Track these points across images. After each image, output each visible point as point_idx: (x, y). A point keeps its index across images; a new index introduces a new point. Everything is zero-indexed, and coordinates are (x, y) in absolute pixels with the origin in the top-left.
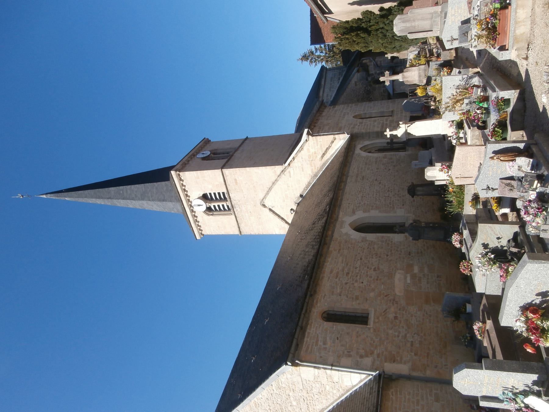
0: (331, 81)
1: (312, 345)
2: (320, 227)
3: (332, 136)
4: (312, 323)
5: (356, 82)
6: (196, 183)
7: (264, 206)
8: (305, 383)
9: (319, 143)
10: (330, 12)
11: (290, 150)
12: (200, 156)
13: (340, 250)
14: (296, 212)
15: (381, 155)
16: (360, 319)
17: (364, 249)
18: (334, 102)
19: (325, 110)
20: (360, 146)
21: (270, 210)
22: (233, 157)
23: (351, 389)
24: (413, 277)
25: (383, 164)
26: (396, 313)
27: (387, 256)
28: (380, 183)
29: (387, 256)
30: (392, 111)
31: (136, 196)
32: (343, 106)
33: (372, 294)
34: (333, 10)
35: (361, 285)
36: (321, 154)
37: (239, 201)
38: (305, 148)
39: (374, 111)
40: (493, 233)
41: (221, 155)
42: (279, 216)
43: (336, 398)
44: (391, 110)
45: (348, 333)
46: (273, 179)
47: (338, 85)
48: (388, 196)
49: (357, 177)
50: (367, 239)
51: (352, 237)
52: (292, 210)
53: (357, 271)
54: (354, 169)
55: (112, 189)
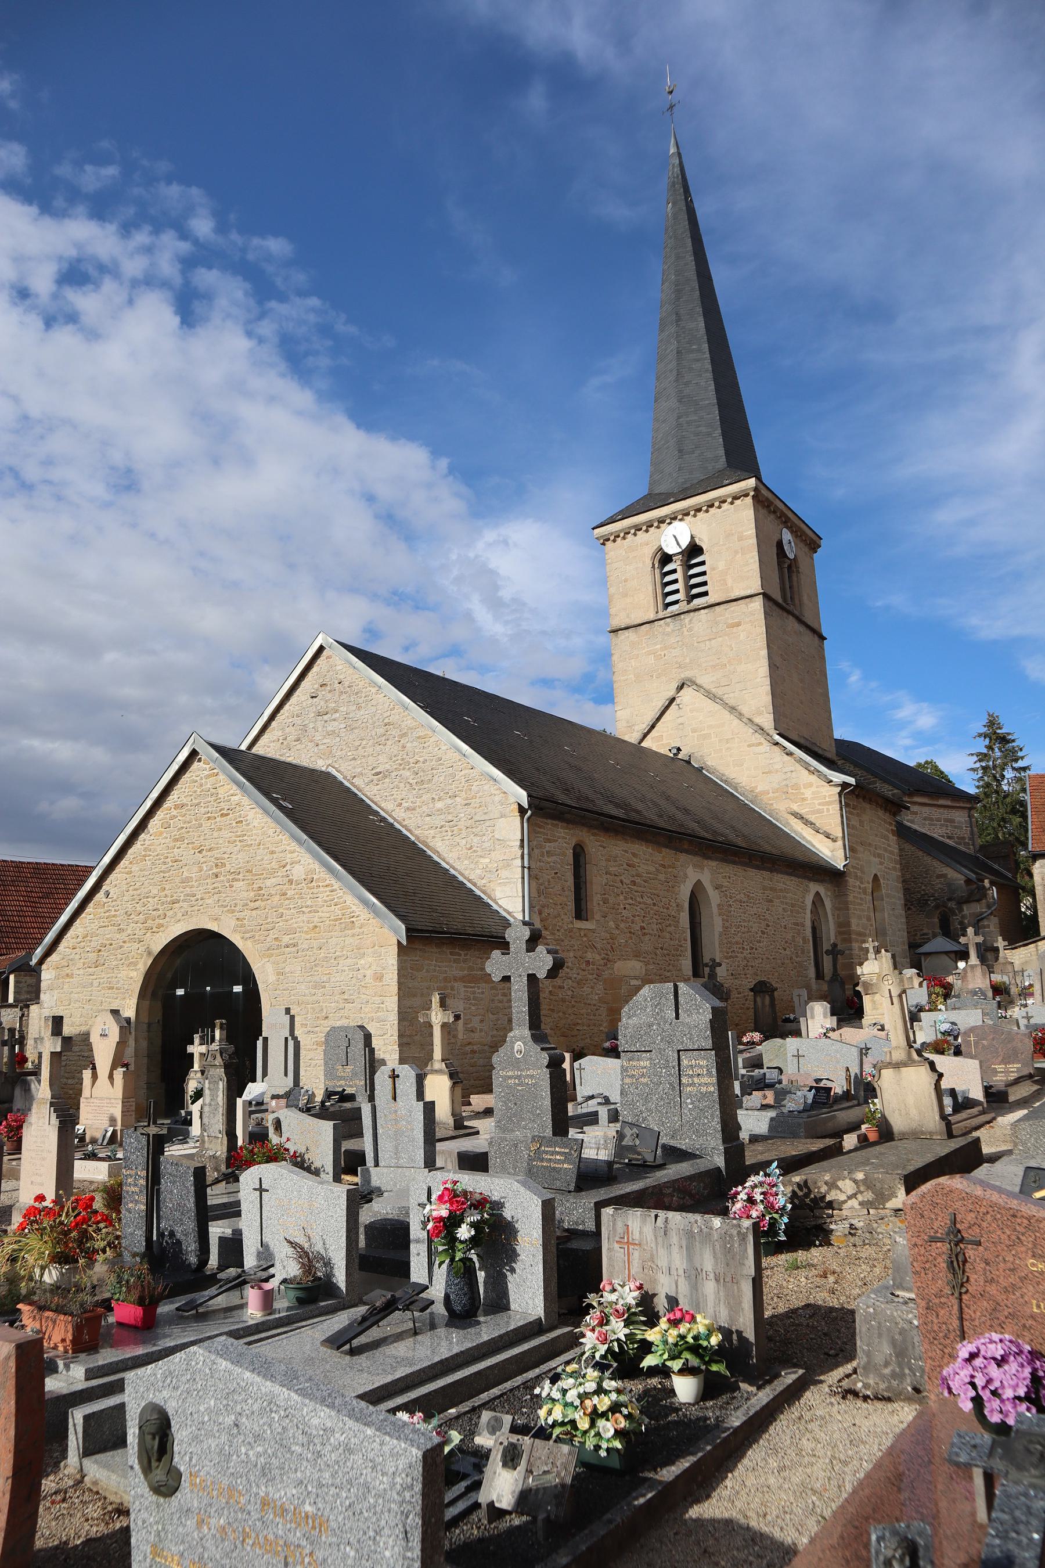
0: (946, 820)
1: (544, 834)
3: (840, 835)
5: (944, 876)
6: (727, 532)
7: (681, 688)
8: (488, 823)
9: (825, 808)
11: (802, 741)
12: (787, 536)
14: (675, 759)
18: (904, 833)
20: (821, 889)
21: (673, 700)
22: (785, 614)
23: (490, 897)
31: (687, 384)
32: (896, 851)
33: (612, 924)
37: (690, 630)
38: (813, 778)
43: (466, 873)
46: (745, 710)
47: (935, 836)
49: (771, 889)
52: (679, 749)
55: (700, 325)
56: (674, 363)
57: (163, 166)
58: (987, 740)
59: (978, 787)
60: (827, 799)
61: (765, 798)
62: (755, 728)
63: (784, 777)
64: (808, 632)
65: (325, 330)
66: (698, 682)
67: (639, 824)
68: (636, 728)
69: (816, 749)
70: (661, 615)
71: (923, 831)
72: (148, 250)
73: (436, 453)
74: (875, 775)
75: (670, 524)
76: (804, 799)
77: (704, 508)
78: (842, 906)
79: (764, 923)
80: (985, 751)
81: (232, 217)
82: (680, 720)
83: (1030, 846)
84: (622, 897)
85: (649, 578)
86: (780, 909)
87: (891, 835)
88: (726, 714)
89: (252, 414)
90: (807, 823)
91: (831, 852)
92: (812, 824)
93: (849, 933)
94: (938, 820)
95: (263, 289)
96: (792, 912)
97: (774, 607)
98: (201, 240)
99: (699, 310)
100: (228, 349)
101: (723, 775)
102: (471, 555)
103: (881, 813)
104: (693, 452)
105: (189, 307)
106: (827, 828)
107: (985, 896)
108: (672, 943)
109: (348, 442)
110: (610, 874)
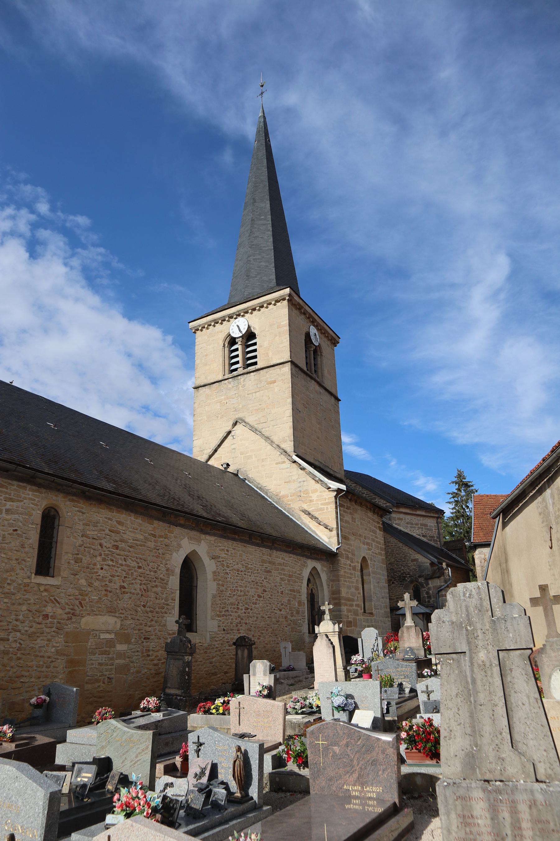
0: (422, 525)
1: (6, 493)
2: (191, 507)
4: (41, 493)
5: (416, 560)
6: (272, 325)
7: (235, 424)
9: (325, 507)
10: (505, 525)
11: (317, 463)
12: (313, 331)
13: (155, 536)
14: (225, 471)
15: (304, 597)
16: (45, 565)
17: (155, 572)
18: (388, 529)
19: (376, 516)
20: (319, 566)
21: (229, 433)
22: (309, 379)
24: (110, 643)
25: (289, 600)
26: (53, 617)
27: (144, 606)
28: (259, 596)
29: (144, 606)
30: (371, 614)
33: (83, 582)
34: (508, 529)
35: (99, 567)
36: (310, 510)
38: (318, 486)
39: (372, 587)
40: (139, 751)
41: (311, 363)
42: (219, 446)
44: (374, 611)
45: (23, 546)
46: (275, 439)
47: (415, 535)
48: (238, 608)
49: (270, 562)
50: (171, 577)
51: (174, 554)
52: (228, 465)
53: (120, 562)
54: (282, 558)
55: (267, 205)
56: (249, 226)
57: (23, 176)
58: (457, 486)
59: (452, 513)
60: (327, 501)
61: (285, 500)
62: (281, 451)
63: (299, 485)
64: (326, 393)
65: (107, 265)
66: (247, 420)
67: (128, 497)
68: (205, 452)
69: (329, 470)
70: (226, 377)
71: (406, 531)
72: (13, 218)
73: (166, 332)
74: (375, 494)
75: (236, 318)
76: (311, 501)
77: (257, 308)
78: (335, 578)
79: (260, 590)
80: (456, 491)
81: (59, 204)
82: (233, 446)
83: (472, 539)
84: (99, 558)
85: (221, 353)
86: (278, 579)
87: (378, 531)
88: (263, 441)
89: (67, 307)
90: (313, 517)
91: (329, 539)
92: (316, 518)
93: (339, 598)
94: (417, 524)
95: (74, 242)
96: (289, 581)
97: (300, 372)
98: (42, 214)
99: (268, 197)
100: (53, 271)
101: (259, 484)
102: (185, 388)
103: (370, 514)
104: (256, 277)
105: (34, 249)
106: (326, 522)
107: (443, 574)
108: (157, 601)
109: (117, 324)
110: (88, 537)
